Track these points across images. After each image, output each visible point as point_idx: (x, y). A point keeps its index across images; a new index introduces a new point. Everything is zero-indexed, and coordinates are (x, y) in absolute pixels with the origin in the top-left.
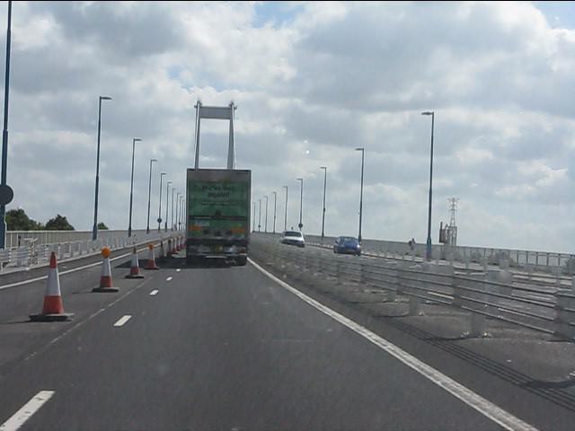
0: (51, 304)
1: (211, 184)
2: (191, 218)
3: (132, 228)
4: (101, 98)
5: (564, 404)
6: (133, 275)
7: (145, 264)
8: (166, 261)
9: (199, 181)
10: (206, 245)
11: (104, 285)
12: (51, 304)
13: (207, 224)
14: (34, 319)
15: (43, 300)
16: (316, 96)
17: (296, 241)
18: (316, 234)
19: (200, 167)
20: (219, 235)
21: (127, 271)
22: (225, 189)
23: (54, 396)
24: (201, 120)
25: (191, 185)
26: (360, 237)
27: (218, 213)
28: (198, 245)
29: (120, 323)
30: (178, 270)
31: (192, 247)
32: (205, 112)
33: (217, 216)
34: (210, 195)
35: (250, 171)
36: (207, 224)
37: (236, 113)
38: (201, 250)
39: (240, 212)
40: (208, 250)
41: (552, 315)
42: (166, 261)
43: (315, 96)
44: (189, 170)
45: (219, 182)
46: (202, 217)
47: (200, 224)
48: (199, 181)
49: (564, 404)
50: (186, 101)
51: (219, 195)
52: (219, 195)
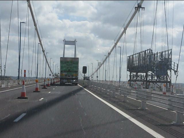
0: (23, 94)
1: (68, 62)
2: (61, 72)
3: (121, 80)
4: (21, 22)
5: (173, 131)
6: (44, 88)
7: (48, 85)
8: (53, 84)
9: (64, 61)
10: (65, 79)
11: (37, 90)
12: (23, 94)
13: (66, 73)
14: (19, 98)
15: (35, 89)
16: (106, 21)
17: (146, 84)
18: (17, 76)
19: (65, 57)
20: (70, 77)
21: (43, 87)
22: (71, 63)
23: (26, 115)
24: (65, 45)
25: (61, 62)
26: (37, 77)
27: (69, 70)
28: (64, 79)
29: (42, 99)
30: (56, 87)
31: (62, 80)
32: (66, 42)
33: (69, 71)
34: (67, 65)
35: (78, 58)
36: (66, 73)
37: (76, 43)
38: (64, 81)
39: (75, 69)
40: (66, 81)
41: (168, 103)
42: (53, 84)
43: (106, 21)
44: (61, 58)
45: (70, 61)
46: (65, 71)
47: (64, 74)
48: (64, 61)
49: (173, 131)
50: (61, 35)
51: (70, 65)
52: (70, 65)
